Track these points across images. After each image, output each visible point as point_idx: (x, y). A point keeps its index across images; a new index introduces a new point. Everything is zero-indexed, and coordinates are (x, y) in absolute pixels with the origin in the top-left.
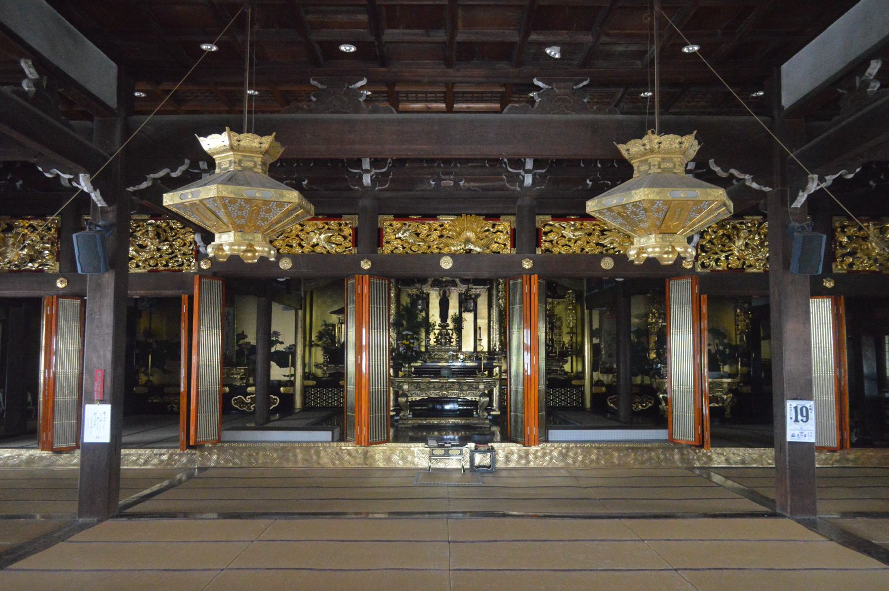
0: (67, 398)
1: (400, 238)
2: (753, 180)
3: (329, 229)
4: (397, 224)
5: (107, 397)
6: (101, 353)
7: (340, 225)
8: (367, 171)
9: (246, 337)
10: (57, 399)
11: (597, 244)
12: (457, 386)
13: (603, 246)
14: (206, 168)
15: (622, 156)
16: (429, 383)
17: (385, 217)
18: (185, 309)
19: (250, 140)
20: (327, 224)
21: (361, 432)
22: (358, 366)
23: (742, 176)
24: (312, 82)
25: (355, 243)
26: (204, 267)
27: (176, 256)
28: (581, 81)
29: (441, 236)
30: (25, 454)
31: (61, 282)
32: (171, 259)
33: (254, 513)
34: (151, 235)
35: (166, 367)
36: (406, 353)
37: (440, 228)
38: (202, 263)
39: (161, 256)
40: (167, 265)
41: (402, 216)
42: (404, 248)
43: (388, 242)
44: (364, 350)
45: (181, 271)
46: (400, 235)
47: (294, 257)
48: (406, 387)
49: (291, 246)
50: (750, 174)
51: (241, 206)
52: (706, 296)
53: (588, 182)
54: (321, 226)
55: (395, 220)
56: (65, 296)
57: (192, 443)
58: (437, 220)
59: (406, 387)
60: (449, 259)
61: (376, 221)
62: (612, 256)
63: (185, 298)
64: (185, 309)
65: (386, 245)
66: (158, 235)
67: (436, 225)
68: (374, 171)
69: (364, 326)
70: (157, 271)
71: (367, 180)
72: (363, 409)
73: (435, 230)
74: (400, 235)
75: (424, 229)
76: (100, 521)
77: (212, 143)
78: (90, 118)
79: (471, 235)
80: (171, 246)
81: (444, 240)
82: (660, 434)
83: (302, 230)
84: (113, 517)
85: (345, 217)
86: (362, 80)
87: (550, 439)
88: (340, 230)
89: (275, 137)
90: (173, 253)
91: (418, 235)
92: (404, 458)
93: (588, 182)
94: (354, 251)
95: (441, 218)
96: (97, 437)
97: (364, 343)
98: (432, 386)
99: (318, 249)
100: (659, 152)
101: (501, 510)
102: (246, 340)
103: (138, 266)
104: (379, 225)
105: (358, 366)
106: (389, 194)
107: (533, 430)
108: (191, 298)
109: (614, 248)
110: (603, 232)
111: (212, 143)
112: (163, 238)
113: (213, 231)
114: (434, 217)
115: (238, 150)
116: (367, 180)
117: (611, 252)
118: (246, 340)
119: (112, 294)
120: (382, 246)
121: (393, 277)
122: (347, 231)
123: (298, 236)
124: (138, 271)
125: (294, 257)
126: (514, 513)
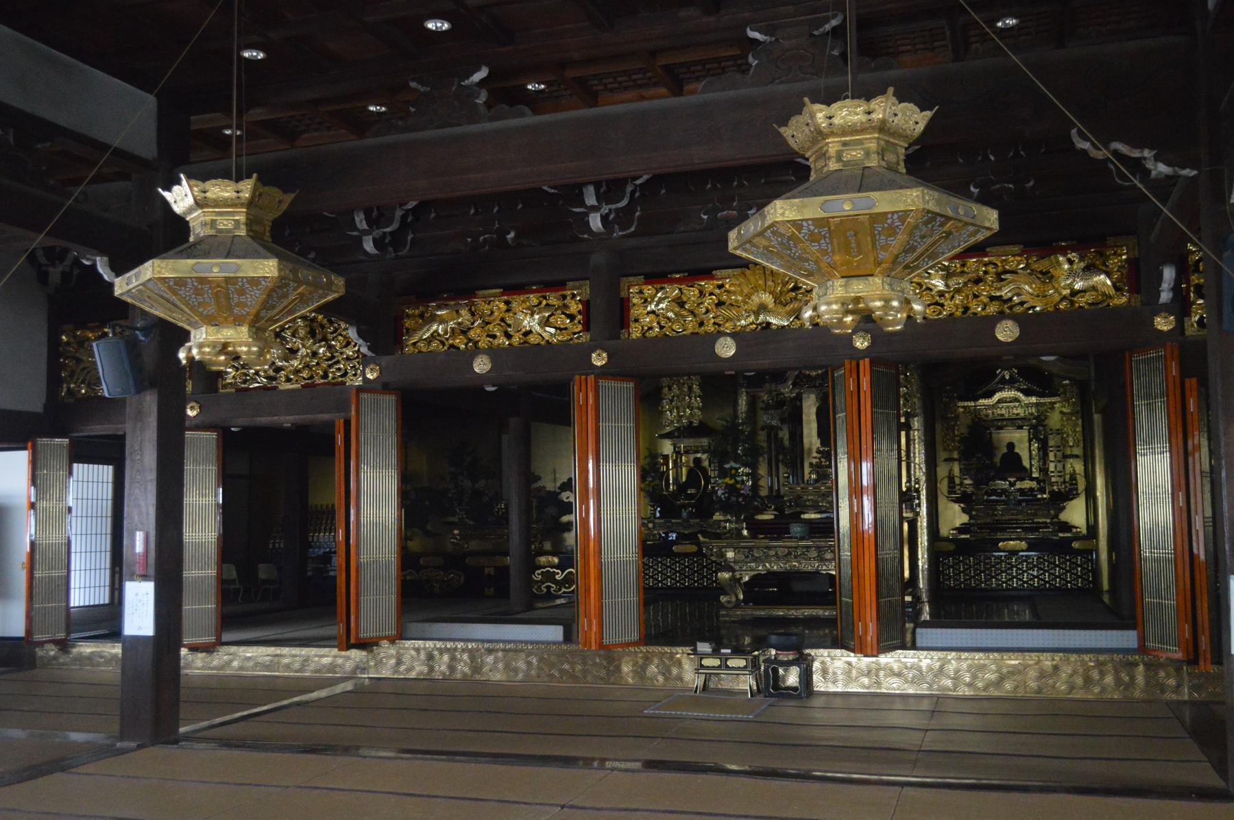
0: (202, 573)
1: (653, 312)
2: (1157, 158)
3: (547, 305)
4: (648, 290)
5: (152, 571)
6: (144, 509)
7: (564, 297)
8: (594, 209)
9: (540, 478)
10: (186, 574)
11: (992, 298)
12: (814, 554)
13: (999, 298)
14: (366, 227)
15: (792, 149)
16: (769, 548)
17: (631, 279)
18: (340, 439)
19: (220, 190)
20: (545, 298)
21: (590, 625)
22: (856, 517)
23: (1136, 154)
24: (413, 84)
25: (587, 327)
26: (369, 376)
27: (338, 362)
28: (827, 20)
29: (720, 304)
30: (291, 656)
31: (192, 408)
32: (330, 366)
33: (549, 757)
34: (302, 332)
35: (429, 527)
36: (728, 499)
37: (717, 291)
38: (367, 370)
39: (318, 364)
40: (325, 376)
41: (657, 277)
42: (662, 328)
43: (636, 321)
44: (591, 495)
45: (344, 383)
46: (652, 307)
47: (493, 352)
48: (730, 555)
49: (494, 337)
50: (1152, 148)
51: (196, 289)
52: (1194, 380)
53: (972, 189)
54: (535, 302)
55: (646, 283)
56: (197, 428)
57: (353, 641)
58: (713, 278)
59: (730, 555)
60: (729, 341)
61: (617, 289)
62: (1015, 317)
63: (340, 423)
64: (340, 439)
65: (632, 325)
66: (312, 333)
67: (709, 286)
68: (605, 209)
69: (590, 457)
70: (313, 385)
71: (595, 222)
72: (592, 590)
73: (711, 294)
74: (652, 307)
75: (692, 293)
76: (140, 747)
77: (180, 197)
78: (126, 177)
79: (767, 298)
80: (330, 347)
81: (723, 311)
82: (1127, 639)
83: (508, 310)
84: (163, 743)
85: (570, 284)
86: (478, 69)
87: (918, 644)
88: (566, 306)
89: (259, 179)
90: (333, 357)
91: (681, 304)
92: (666, 673)
93: (972, 189)
94: (585, 338)
95: (718, 273)
96: (140, 628)
97: (591, 485)
98: (772, 553)
99: (532, 339)
100: (832, 134)
101: (710, 761)
102: (540, 484)
103: (288, 380)
104: (623, 294)
105: (856, 517)
106: (633, 242)
107: (870, 628)
108: (347, 423)
109: (1022, 303)
110: (999, 277)
111: (180, 197)
112: (319, 337)
113: (187, 328)
114: (707, 274)
115: (207, 206)
116: (595, 222)
117: (1018, 309)
118: (540, 484)
119: (155, 424)
120: (628, 327)
121: (694, 374)
122: (574, 307)
123: (502, 320)
124: (289, 386)
125: (493, 352)
126: (734, 767)
